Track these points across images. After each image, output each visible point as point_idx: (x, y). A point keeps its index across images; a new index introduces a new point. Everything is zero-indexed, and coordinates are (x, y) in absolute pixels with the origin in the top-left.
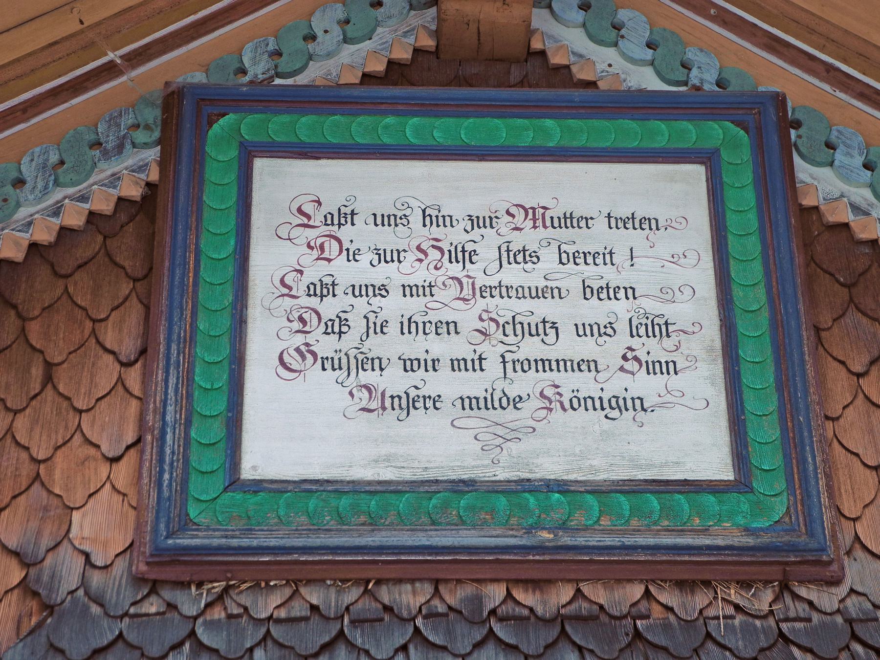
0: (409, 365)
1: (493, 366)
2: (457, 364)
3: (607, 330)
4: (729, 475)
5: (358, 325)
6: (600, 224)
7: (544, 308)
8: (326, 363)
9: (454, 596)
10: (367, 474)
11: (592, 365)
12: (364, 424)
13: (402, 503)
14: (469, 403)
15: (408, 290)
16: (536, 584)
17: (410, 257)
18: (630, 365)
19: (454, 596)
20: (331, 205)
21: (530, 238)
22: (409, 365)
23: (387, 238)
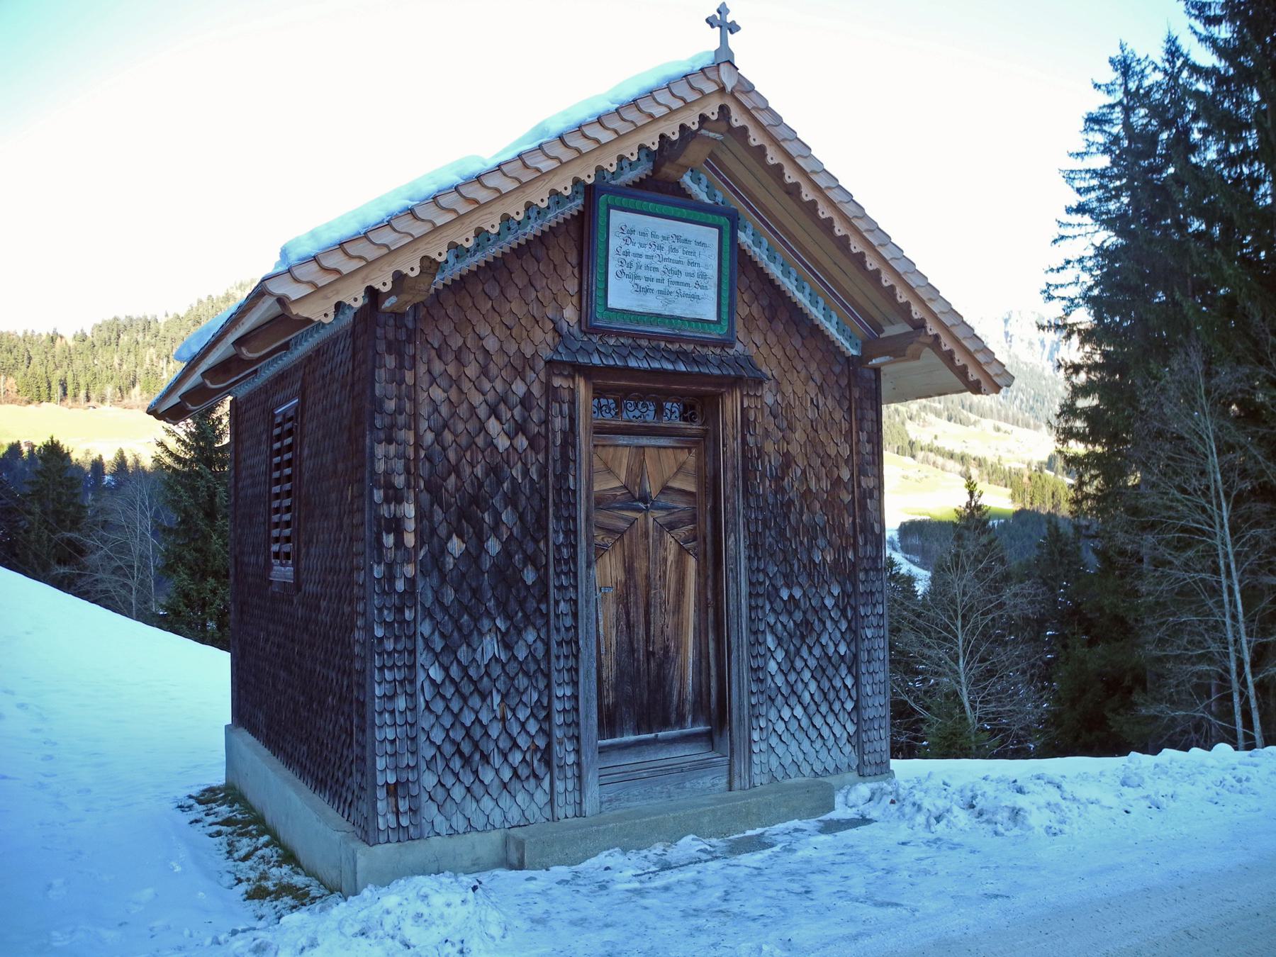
0: (647, 279)
1: (666, 281)
2: (658, 280)
3: (691, 275)
4: (715, 319)
5: (635, 265)
6: (693, 243)
7: (679, 267)
8: (628, 276)
9: (654, 343)
10: (636, 309)
11: (687, 285)
12: (635, 295)
13: (645, 318)
14: (660, 292)
15: (647, 256)
16: (671, 342)
17: (648, 246)
18: (556, 819)
19: (654, 343)
20: (628, 228)
21: (677, 245)
22: (647, 279)
23: (643, 240)
